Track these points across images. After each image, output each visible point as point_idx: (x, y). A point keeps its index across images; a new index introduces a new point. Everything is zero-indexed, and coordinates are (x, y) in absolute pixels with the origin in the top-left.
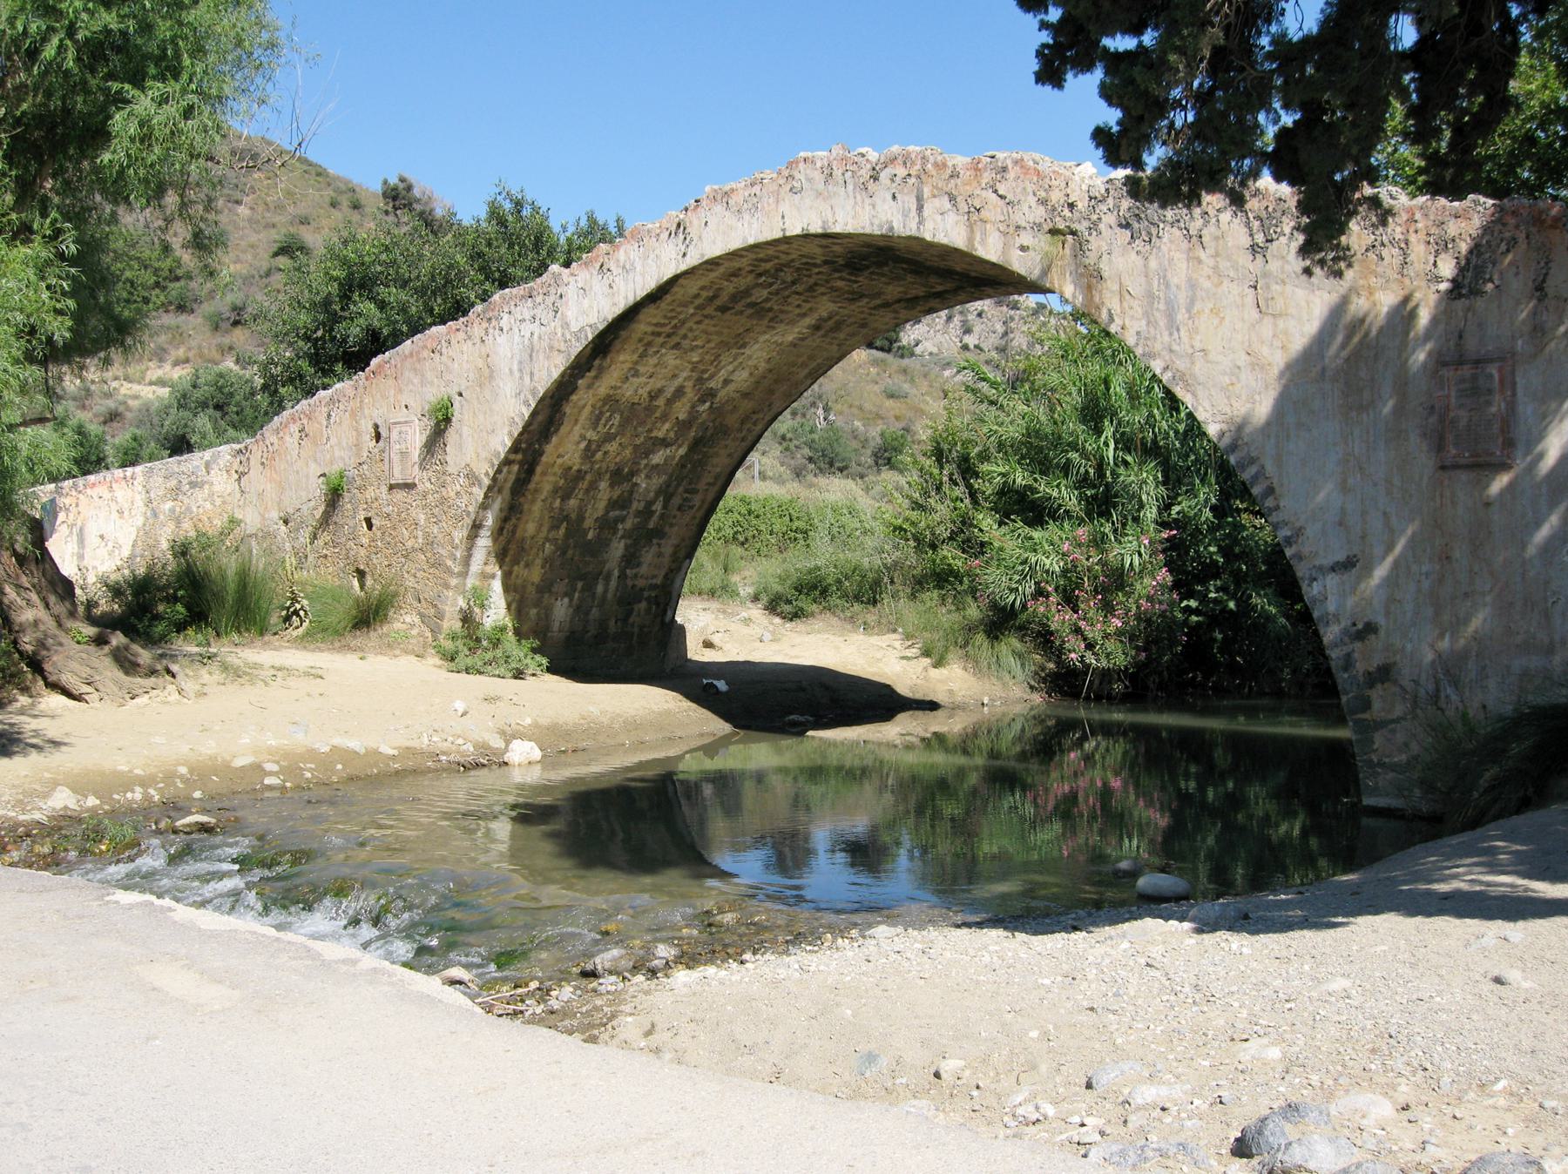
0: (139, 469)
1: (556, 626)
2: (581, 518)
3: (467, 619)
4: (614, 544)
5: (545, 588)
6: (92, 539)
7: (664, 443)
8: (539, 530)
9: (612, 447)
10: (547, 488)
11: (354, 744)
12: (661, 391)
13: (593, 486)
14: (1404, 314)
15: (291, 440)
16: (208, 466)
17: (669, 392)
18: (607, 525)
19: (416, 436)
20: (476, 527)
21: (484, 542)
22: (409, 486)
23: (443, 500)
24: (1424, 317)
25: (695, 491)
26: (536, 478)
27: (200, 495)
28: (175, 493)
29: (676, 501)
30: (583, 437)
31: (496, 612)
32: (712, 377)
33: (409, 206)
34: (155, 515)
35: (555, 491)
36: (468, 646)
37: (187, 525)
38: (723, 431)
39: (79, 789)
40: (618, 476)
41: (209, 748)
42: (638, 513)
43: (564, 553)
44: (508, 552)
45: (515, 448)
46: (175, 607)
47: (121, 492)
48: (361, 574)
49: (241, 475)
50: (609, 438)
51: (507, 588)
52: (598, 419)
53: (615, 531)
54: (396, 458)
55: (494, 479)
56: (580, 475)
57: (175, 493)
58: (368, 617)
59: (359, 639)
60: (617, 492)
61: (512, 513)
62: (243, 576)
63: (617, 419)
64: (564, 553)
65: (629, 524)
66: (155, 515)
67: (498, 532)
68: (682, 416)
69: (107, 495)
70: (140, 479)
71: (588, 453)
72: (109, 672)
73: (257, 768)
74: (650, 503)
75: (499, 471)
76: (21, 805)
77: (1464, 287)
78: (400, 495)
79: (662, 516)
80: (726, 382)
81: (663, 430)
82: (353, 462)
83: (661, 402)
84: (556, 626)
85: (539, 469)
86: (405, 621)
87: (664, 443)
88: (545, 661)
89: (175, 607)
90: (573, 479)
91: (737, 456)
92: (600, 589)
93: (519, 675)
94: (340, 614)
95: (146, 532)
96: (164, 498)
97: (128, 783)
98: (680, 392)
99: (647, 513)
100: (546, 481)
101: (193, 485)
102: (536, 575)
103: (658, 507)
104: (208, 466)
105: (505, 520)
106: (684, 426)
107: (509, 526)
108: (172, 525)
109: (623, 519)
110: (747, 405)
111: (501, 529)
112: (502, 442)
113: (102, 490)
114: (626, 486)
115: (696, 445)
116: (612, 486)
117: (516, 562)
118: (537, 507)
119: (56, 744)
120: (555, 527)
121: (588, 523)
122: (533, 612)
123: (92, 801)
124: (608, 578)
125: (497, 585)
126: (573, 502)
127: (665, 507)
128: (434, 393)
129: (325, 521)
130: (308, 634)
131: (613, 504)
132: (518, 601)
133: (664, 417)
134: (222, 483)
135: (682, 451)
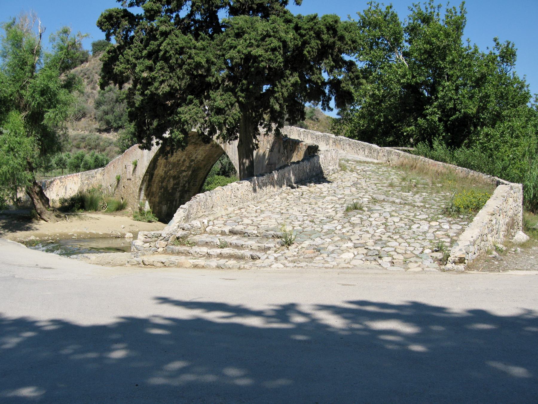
0: (79, 173)
1: (163, 211)
2: (167, 187)
3: (141, 209)
4: (177, 193)
5: (160, 203)
6: (68, 189)
7: (184, 171)
8: (157, 189)
9: (172, 172)
10: (157, 181)
11: (94, 232)
12: (180, 160)
13: (169, 180)
14: (264, 155)
15: (112, 168)
16: (96, 173)
17: (182, 160)
18: (174, 189)
19: (131, 168)
20: (141, 189)
21: (143, 192)
22: (130, 179)
23: (135, 183)
24: (266, 157)
25: (196, 182)
26: (154, 178)
27: (94, 179)
28: (88, 179)
29: (191, 184)
30: (163, 170)
31: (147, 207)
32: (192, 157)
33: (395, 22)
34: (83, 184)
35: (159, 181)
36: (141, 215)
37: (91, 186)
38: (199, 168)
39: (36, 236)
40: (174, 178)
41: (66, 231)
42: (182, 187)
43: (164, 195)
44: (149, 195)
45: (147, 172)
46: (78, 205)
47: (76, 179)
48: (122, 198)
49: (104, 175)
50: (170, 170)
51: (150, 203)
52: (166, 165)
53: (177, 191)
54: (128, 173)
55: (143, 179)
56: (165, 178)
57: (88, 179)
58: (120, 208)
59: (119, 213)
60: (175, 182)
61: (149, 186)
62: (92, 198)
63: (171, 166)
64: (164, 195)
65: (180, 189)
66: (83, 184)
67: (146, 190)
68: (188, 165)
69: (72, 179)
70: (80, 176)
71: (166, 173)
72: (53, 217)
73: (73, 235)
74: (184, 184)
75: (144, 177)
76: (25, 238)
77: (271, 151)
78: (129, 181)
79: (188, 187)
80: (196, 158)
81: (183, 168)
82: (121, 173)
83: (181, 162)
84: (163, 211)
85: (154, 177)
86: (129, 209)
87: (184, 171)
88: (158, 219)
89: (78, 205)
90: (163, 179)
91: (205, 174)
92: (174, 203)
93: (150, 222)
94: (114, 206)
95: (81, 187)
96: (85, 180)
97: (46, 236)
98: (185, 160)
99: (184, 186)
100: (156, 179)
101: (92, 177)
102: (157, 200)
103: (187, 185)
104: (96, 173)
105: (148, 187)
106: (189, 167)
107: (149, 189)
108: (87, 186)
109: (178, 188)
110: (204, 163)
111: (147, 190)
112: (144, 171)
113: (71, 178)
114: (177, 180)
115: (193, 171)
116: (174, 180)
117: (152, 197)
118: (155, 185)
119: (37, 229)
120: (160, 189)
121: (169, 188)
122: (157, 208)
123: (38, 238)
124: (176, 201)
125: (147, 202)
126: (164, 184)
127: (189, 185)
128: (134, 159)
129: (117, 186)
130: (107, 211)
131: (174, 184)
132: (153, 205)
133: (183, 165)
134: (99, 176)
135: (190, 173)
